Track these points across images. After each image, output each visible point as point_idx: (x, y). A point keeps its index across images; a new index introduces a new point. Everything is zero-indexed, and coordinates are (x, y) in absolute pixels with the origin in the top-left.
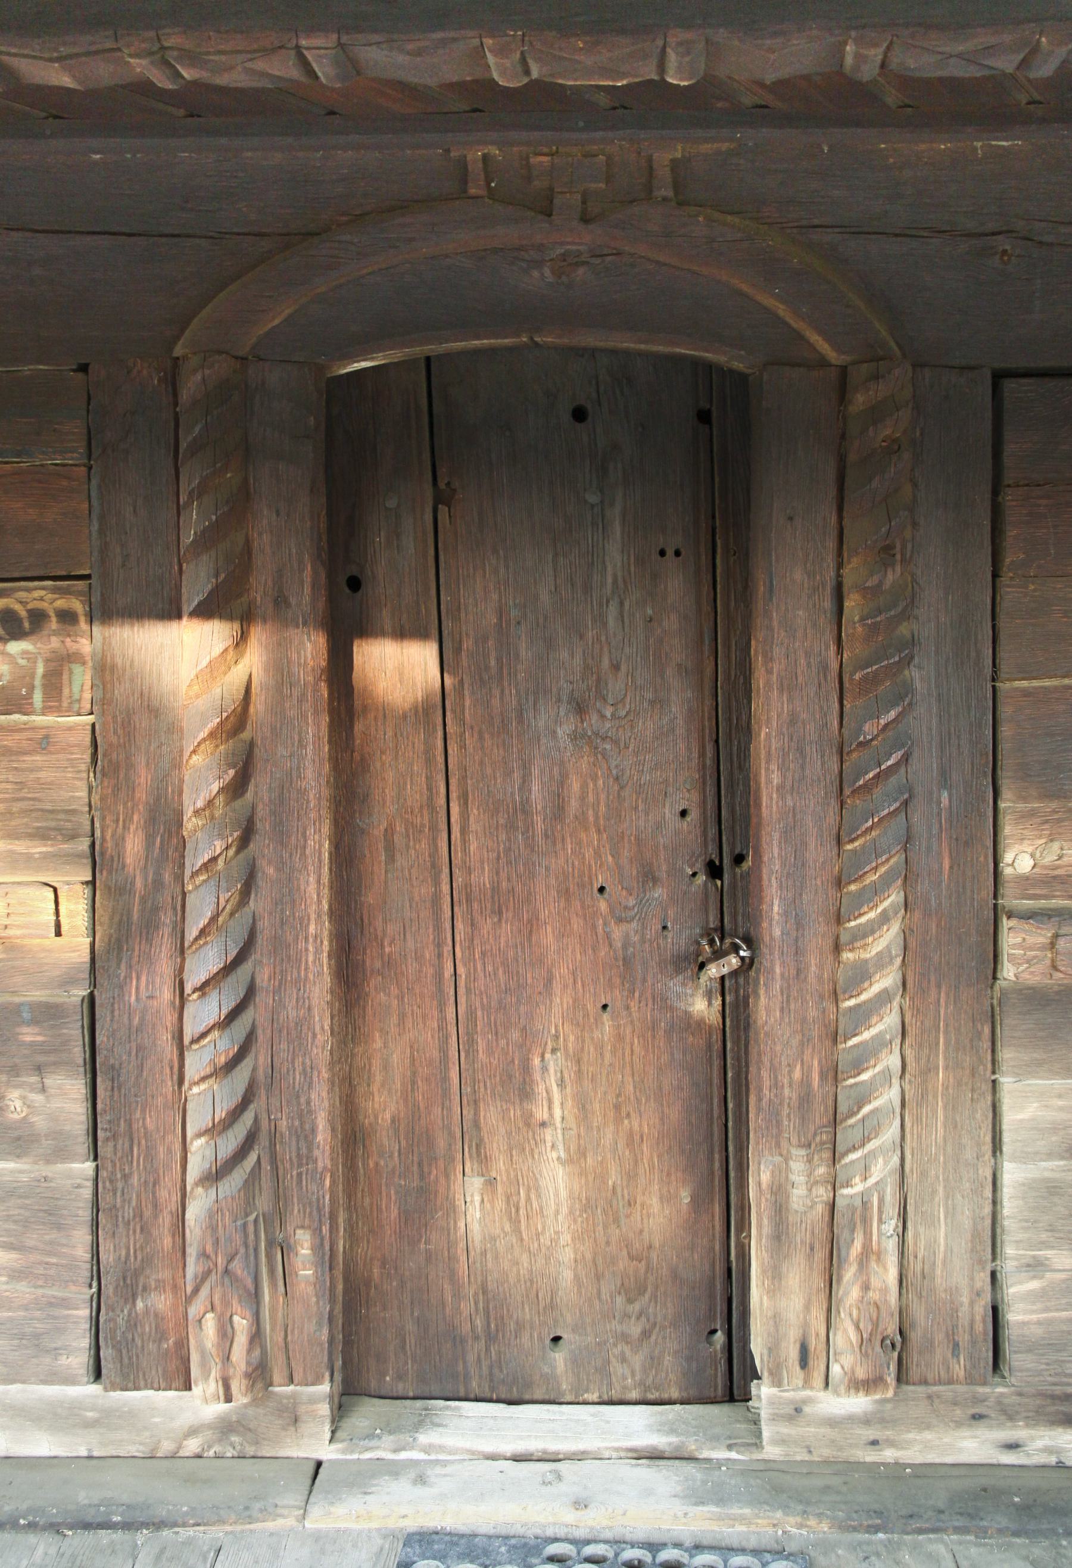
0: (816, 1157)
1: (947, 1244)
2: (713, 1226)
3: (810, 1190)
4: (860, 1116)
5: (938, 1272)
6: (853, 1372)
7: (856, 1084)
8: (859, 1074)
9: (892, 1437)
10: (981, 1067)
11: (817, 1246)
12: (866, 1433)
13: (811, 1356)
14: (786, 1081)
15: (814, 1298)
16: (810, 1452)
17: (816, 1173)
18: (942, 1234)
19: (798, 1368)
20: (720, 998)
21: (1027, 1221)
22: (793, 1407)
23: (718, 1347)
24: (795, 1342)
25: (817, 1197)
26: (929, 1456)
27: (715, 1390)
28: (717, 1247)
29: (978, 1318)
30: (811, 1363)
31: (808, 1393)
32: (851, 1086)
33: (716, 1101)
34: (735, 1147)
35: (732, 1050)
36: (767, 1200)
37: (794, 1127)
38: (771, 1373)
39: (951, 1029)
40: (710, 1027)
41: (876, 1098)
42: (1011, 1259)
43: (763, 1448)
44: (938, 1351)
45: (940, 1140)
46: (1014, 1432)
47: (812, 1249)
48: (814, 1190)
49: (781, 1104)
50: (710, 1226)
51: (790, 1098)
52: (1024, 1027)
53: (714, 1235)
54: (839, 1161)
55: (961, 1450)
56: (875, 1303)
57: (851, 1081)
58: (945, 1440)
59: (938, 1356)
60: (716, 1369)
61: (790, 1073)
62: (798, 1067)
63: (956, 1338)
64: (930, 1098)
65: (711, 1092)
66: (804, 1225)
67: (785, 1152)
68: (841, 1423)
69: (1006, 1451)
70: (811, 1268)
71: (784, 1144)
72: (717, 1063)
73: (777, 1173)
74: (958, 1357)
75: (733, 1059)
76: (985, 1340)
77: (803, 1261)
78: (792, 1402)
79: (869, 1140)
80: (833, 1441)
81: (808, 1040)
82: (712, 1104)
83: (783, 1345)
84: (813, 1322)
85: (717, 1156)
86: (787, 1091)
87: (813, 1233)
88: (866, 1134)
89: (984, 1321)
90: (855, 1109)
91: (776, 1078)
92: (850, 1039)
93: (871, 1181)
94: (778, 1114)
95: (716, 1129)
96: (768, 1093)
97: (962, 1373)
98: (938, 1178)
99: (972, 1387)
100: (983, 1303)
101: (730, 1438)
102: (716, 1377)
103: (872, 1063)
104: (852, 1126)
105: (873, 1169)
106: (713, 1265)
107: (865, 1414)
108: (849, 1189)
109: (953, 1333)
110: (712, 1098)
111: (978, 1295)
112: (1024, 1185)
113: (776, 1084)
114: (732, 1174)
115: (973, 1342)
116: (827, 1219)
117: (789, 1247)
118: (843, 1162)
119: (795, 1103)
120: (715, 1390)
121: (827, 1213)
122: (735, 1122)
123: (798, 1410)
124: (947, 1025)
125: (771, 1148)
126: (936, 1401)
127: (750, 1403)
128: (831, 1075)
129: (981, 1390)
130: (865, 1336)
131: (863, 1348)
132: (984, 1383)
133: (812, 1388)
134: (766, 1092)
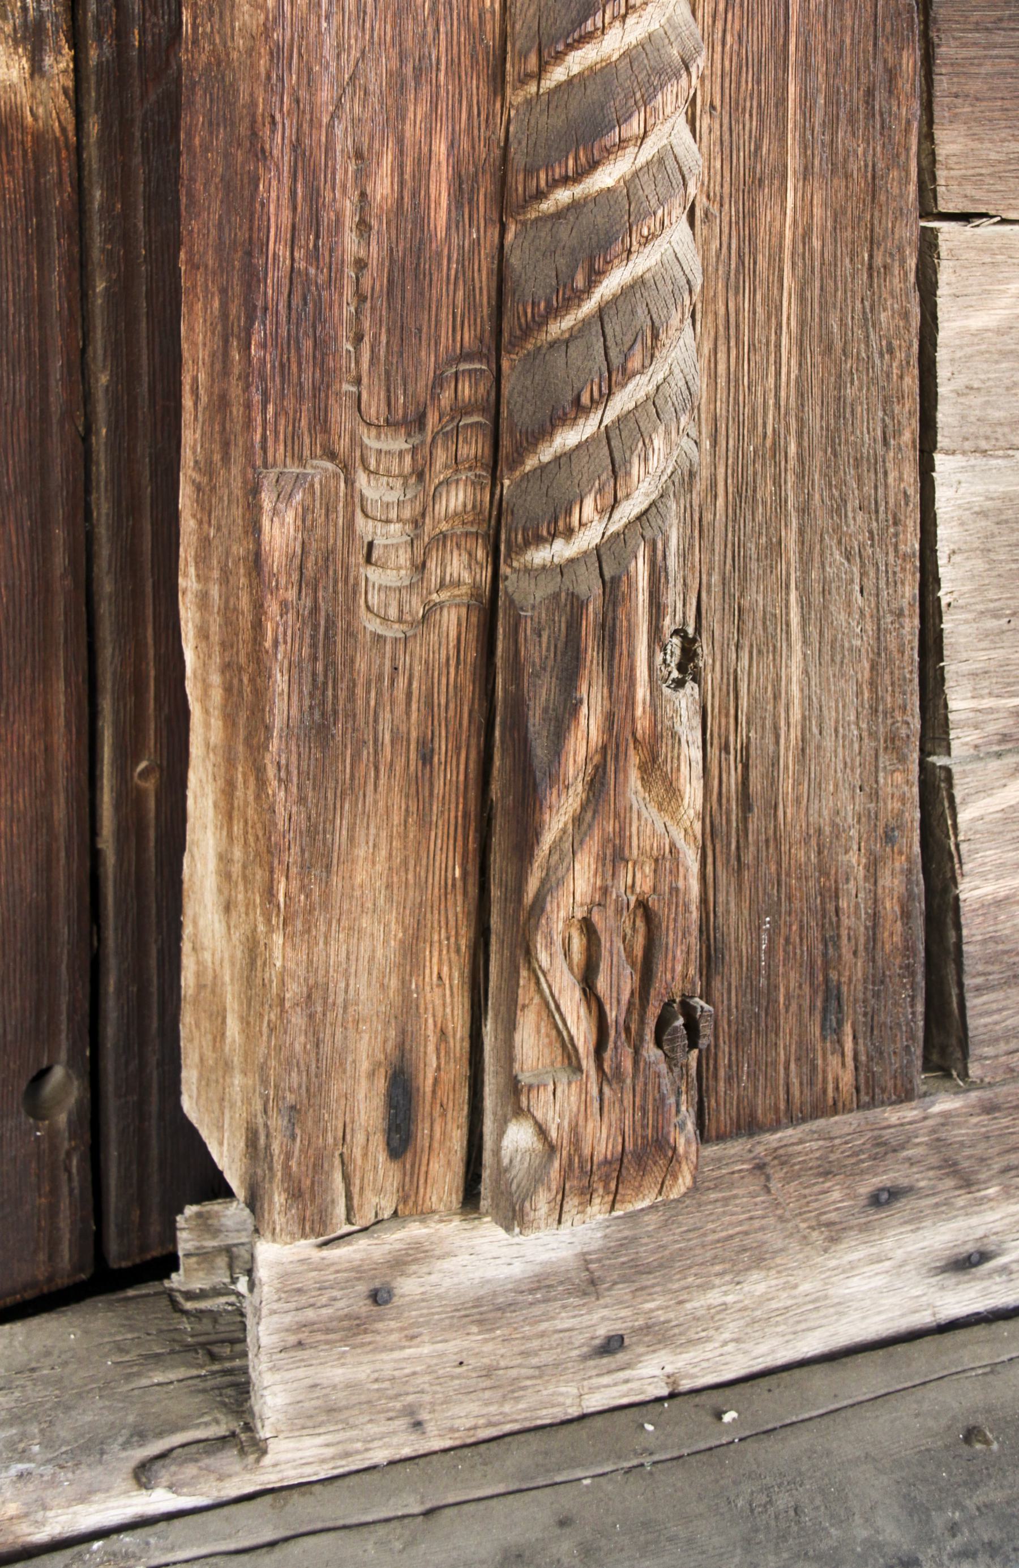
0: (441, 457)
1: (807, 699)
2: (48, 749)
3: (420, 567)
4: (589, 307)
5: (787, 786)
6: (576, 1141)
7: (575, 206)
8: (593, 165)
9: (662, 1316)
10: (895, 174)
11: (442, 747)
12: (587, 1320)
13: (424, 1107)
14: (348, 207)
15: (433, 918)
16: (418, 1425)
17: (440, 508)
18: (796, 673)
19: (382, 1157)
20: (67, 52)
21: (996, 615)
22: (363, 1288)
23: (62, 1119)
24: (372, 1075)
25: (442, 585)
26: (763, 1348)
27: (52, 1256)
28: (60, 813)
29: (890, 907)
30: (423, 1131)
31: (415, 1230)
32: (559, 214)
33: (57, 365)
34: (117, 503)
35: (107, 209)
36: (284, 605)
37: (373, 360)
38: (295, 1194)
39: (818, 60)
40: (38, 137)
41: (647, 240)
42: (963, 725)
43: (260, 1449)
44: (788, 1023)
45: (788, 395)
46: (974, 1221)
47: (426, 757)
48: (432, 565)
49: (334, 281)
50: (39, 748)
51: (361, 265)
52: (987, 68)
53: (49, 779)
54: (517, 460)
55: (841, 1307)
56: (642, 904)
57: (563, 196)
58: (805, 1287)
59: (785, 1044)
60: (54, 1191)
61: (362, 175)
62: (388, 160)
63: (833, 975)
64: (762, 263)
65: (43, 343)
66: (402, 683)
67: (342, 446)
68: (511, 1306)
69: (950, 1279)
70: (424, 822)
71: (341, 417)
72: (59, 247)
73: (319, 512)
74: (838, 1031)
75: (108, 238)
76: (909, 969)
77: (397, 801)
78: (358, 1272)
79: (628, 376)
80: (489, 1372)
81: (418, 73)
82: (45, 375)
83: (336, 1088)
84: (432, 997)
85: (59, 533)
86: (350, 243)
87: (430, 704)
88: (616, 361)
89: (906, 915)
90: (580, 282)
91: (314, 195)
92: (559, 57)
93: (629, 510)
94: (319, 317)
95: (57, 449)
96: (284, 252)
97: (847, 1078)
98: (781, 502)
99: (872, 1114)
100: (900, 863)
101: (140, 1435)
102: (53, 1211)
103: (634, 126)
104: (566, 342)
105: (636, 468)
106: (47, 866)
107: (585, 1260)
108: (559, 544)
109: (826, 965)
110: (44, 358)
111: (889, 838)
112: (983, 514)
113: (315, 221)
114: (106, 586)
115: (877, 980)
116: (471, 655)
117: (356, 757)
118: (530, 463)
119: (374, 279)
120: (52, 1256)
121: (471, 637)
122: (114, 428)
123: (379, 1297)
124: (807, 50)
125: (295, 435)
126: (777, 1174)
127: (177, 1280)
128: (486, 187)
129: (893, 1115)
130: (611, 1015)
131: (608, 1055)
132: (906, 1095)
133: (424, 1215)
134: (278, 248)
